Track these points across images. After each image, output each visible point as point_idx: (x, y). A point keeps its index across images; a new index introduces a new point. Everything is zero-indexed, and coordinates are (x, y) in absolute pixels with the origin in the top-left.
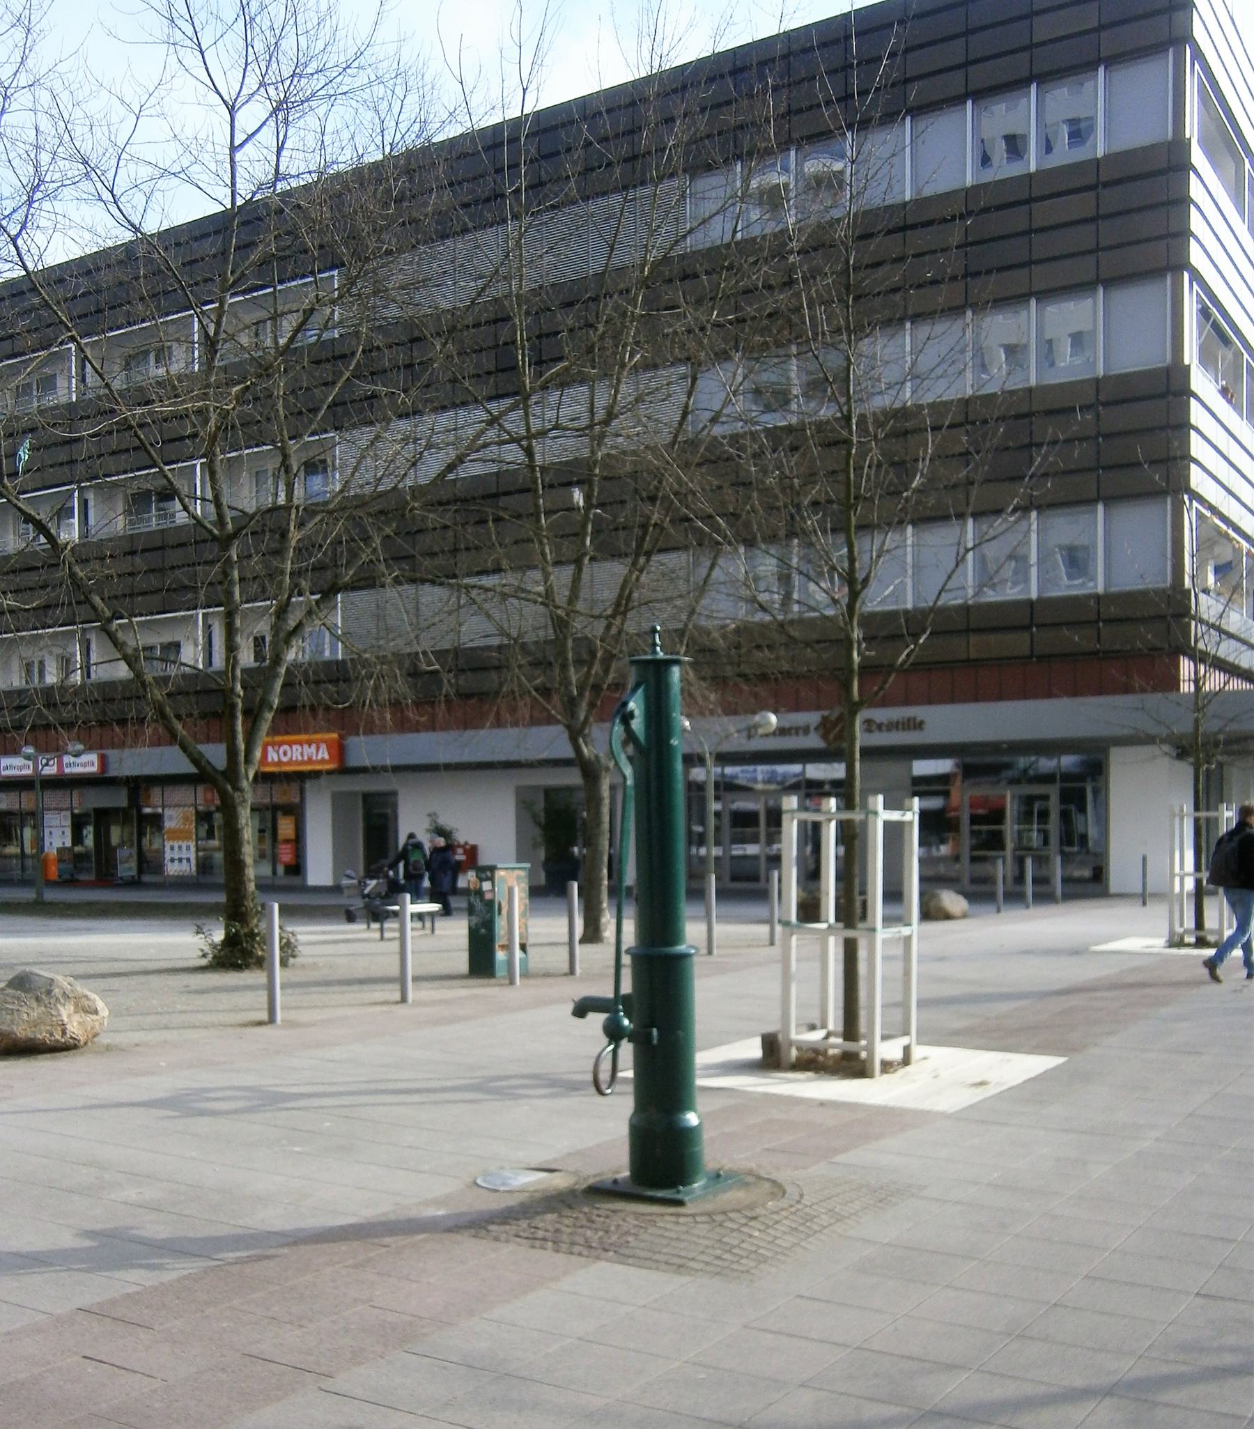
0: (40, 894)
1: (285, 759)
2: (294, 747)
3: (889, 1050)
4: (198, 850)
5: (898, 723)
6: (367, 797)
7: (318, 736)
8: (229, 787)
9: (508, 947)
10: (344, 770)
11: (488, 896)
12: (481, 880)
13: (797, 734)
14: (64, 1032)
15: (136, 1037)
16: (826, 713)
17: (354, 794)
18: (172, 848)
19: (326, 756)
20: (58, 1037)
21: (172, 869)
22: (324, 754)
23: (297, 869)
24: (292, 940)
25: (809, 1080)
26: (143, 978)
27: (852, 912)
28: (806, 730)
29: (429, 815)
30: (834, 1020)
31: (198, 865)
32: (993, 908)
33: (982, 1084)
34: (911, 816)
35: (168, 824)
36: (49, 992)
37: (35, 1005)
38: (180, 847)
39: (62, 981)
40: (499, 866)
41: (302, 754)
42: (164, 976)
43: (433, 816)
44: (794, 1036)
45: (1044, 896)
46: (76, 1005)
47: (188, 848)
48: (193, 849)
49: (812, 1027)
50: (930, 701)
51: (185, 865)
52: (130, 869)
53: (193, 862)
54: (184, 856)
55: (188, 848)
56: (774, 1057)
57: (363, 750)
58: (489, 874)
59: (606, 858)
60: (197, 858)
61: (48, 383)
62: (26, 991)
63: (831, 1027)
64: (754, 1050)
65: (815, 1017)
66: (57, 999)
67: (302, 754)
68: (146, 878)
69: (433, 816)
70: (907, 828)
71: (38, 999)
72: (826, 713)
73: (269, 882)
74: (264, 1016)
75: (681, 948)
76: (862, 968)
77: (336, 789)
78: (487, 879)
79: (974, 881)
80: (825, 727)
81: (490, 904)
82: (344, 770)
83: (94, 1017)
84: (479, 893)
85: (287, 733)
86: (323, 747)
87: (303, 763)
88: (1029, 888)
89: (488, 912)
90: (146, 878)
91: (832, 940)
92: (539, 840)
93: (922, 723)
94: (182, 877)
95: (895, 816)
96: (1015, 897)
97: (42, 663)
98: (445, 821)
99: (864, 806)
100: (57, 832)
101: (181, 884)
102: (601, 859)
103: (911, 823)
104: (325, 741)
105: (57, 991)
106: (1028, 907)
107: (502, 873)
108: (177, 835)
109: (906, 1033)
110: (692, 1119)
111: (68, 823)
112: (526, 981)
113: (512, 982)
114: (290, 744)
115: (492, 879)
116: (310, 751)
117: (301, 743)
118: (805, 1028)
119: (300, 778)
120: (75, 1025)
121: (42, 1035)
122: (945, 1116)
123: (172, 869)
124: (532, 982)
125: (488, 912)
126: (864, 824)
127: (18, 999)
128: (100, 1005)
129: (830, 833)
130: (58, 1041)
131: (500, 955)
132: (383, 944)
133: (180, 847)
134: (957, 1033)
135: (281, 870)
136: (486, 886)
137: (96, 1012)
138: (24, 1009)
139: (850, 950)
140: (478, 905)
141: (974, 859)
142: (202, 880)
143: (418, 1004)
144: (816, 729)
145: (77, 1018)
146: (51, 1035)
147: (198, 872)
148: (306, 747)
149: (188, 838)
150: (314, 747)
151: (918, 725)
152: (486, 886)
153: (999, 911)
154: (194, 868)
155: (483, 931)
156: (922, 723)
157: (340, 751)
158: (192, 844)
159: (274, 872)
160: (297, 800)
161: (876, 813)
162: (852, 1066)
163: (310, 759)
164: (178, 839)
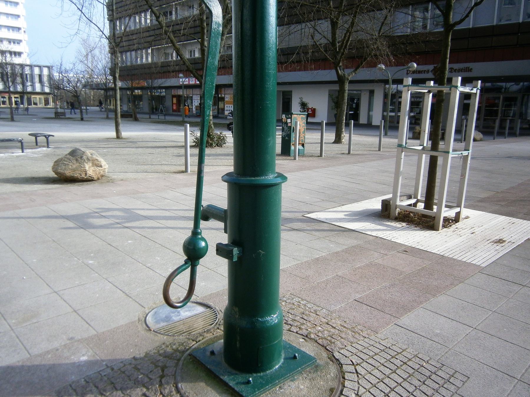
0: (183, 119)
3: (448, 213)
5: (462, 69)
9: (295, 145)
12: (287, 118)
13: (424, 73)
14: (86, 174)
15: (122, 176)
16: (436, 65)
20: (83, 176)
25: (402, 229)
26: (164, 150)
27: (438, 135)
28: (428, 72)
30: (421, 194)
32: (492, 138)
33: (500, 241)
34: (475, 90)
35: (226, 100)
36: (81, 157)
37: (75, 162)
39: (88, 152)
42: (177, 149)
43: (301, 98)
44: (398, 203)
45: (512, 134)
46: (93, 163)
49: (410, 197)
50: (475, 61)
56: (386, 213)
59: (345, 113)
62: (73, 156)
63: (419, 198)
64: (378, 206)
65: (411, 191)
66: (84, 160)
68: (220, 116)
69: (301, 98)
70: (472, 97)
71: (77, 160)
72: (436, 65)
74: (183, 168)
75: (270, 178)
76: (437, 189)
79: (484, 127)
80: (435, 71)
84: (286, 123)
88: (507, 132)
90: (220, 116)
91: (424, 155)
92: (334, 107)
93: (471, 69)
95: (467, 90)
96: (501, 134)
97: (194, 51)
98: (305, 100)
99: (450, 80)
100: (196, 101)
102: (343, 113)
103: (476, 94)
105: (84, 157)
106: (505, 138)
107: (295, 116)
108: (228, 103)
109: (459, 206)
110: (273, 319)
111: (199, 98)
113: (295, 159)
118: (405, 197)
120: (90, 170)
121: (77, 175)
122: (480, 270)
126: (449, 94)
127: (70, 159)
128: (103, 163)
129: (429, 100)
130: (83, 178)
131: (292, 148)
134: (482, 200)
136: (289, 121)
137: (101, 166)
138: (71, 164)
139: (433, 162)
140: (286, 128)
141: (485, 120)
144: (431, 71)
145: (92, 168)
146: (81, 175)
149: (231, 104)
151: (470, 70)
152: (289, 121)
153: (494, 139)
156: (471, 69)
161: (456, 87)
162: (428, 223)
164: (229, 104)
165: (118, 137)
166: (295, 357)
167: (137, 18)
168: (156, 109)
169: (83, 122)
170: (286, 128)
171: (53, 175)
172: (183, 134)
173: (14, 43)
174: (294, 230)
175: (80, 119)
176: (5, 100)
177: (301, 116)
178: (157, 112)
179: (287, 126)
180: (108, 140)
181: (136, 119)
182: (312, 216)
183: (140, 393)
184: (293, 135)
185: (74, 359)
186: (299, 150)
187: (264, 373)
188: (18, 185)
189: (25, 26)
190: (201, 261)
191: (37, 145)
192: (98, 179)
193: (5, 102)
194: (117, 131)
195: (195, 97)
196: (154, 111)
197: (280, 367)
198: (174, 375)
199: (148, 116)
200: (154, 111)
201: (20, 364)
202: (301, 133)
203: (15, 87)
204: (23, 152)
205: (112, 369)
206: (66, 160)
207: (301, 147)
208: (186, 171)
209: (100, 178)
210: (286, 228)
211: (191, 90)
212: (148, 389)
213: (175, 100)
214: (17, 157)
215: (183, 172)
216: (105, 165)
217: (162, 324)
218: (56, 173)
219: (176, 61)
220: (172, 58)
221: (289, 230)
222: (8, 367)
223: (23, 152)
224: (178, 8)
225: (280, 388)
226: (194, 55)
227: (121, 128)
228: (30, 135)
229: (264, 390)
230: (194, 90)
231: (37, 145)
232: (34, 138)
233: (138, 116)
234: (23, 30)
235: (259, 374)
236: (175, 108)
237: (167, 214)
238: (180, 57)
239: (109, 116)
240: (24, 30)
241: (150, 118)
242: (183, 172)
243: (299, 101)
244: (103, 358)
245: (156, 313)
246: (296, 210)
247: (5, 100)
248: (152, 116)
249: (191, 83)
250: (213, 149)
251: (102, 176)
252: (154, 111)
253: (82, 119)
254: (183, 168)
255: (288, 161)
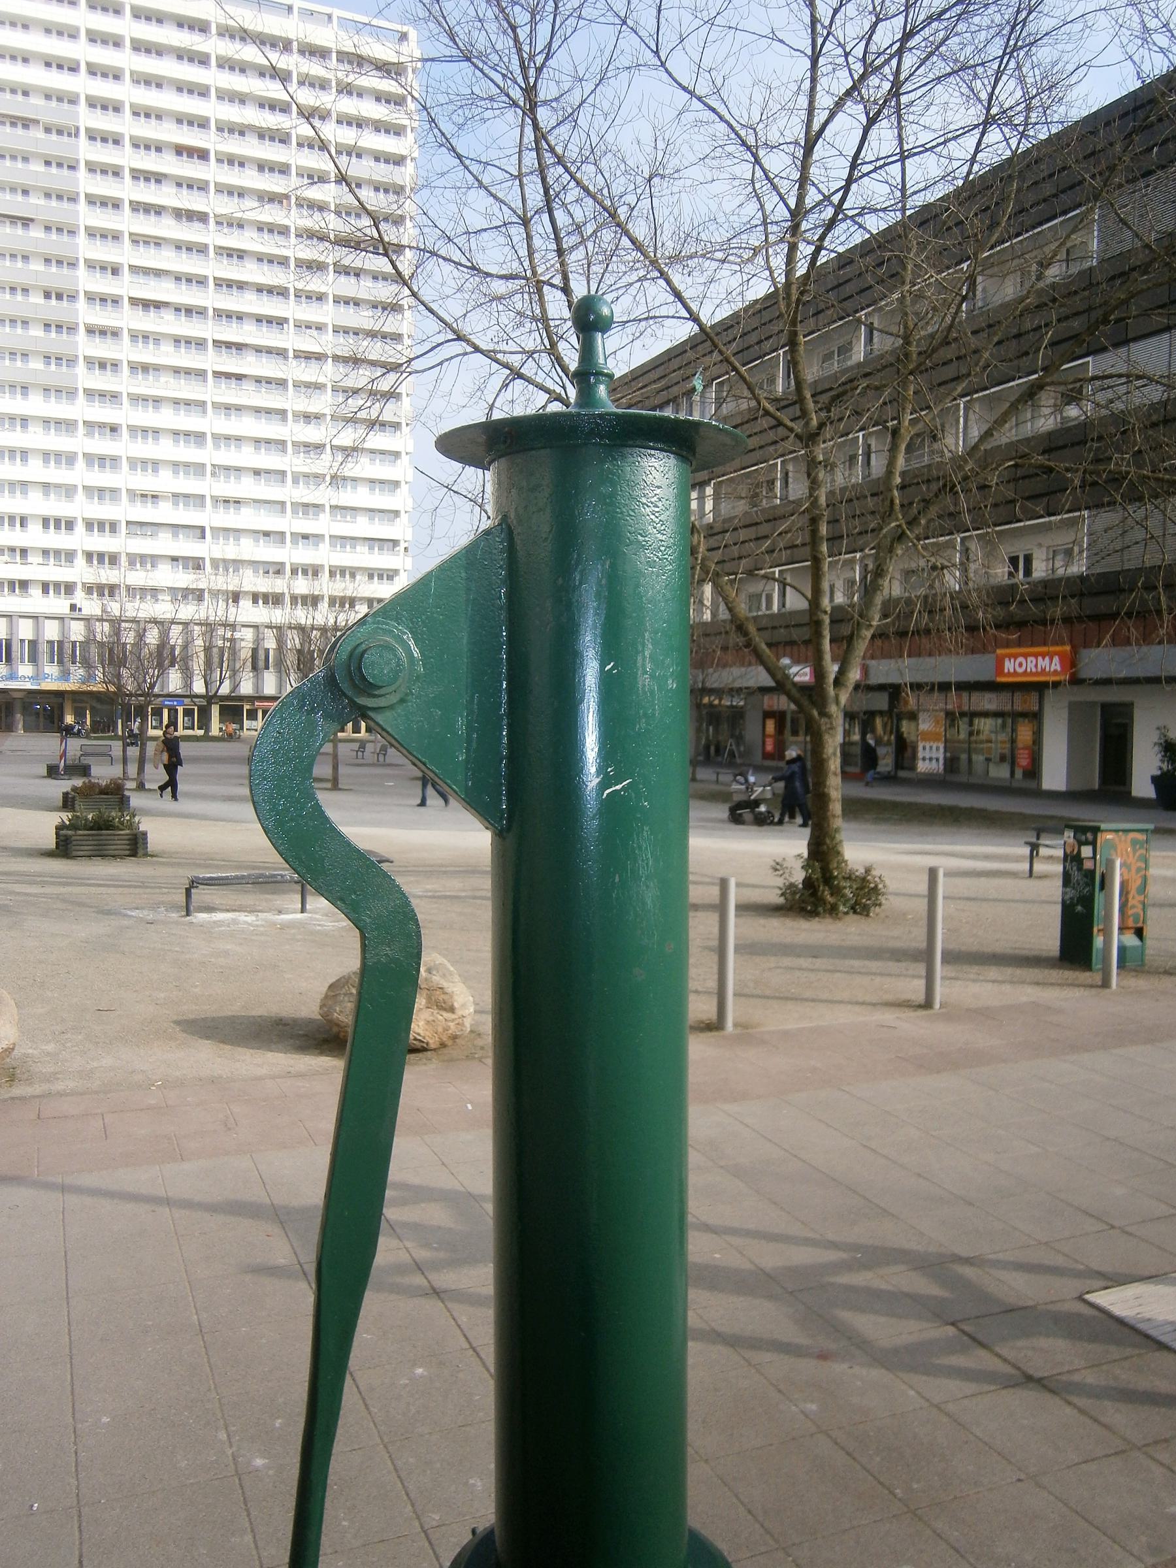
1: (1020, 670)
2: (1029, 659)
4: (945, 751)
6: (1106, 708)
7: (1052, 649)
8: (815, 713)
10: (1076, 681)
11: (1088, 865)
12: (1081, 843)
17: (1092, 704)
18: (924, 748)
19: (1059, 669)
21: (922, 767)
22: (1056, 665)
23: (1034, 772)
24: (880, 886)
29: (1158, 728)
31: (945, 764)
38: (931, 748)
40: (1103, 826)
41: (1036, 666)
43: (1163, 730)
47: (938, 749)
48: (942, 750)
51: (934, 764)
52: (887, 765)
53: (941, 761)
54: (934, 756)
55: (938, 749)
57: (1101, 660)
58: (1090, 836)
60: (945, 759)
61: (845, 350)
67: (1036, 666)
68: (902, 774)
69: (1163, 730)
73: (1008, 784)
77: (1073, 699)
78: (1087, 843)
81: (1091, 874)
82: (1076, 681)
83: (447, 1015)
85: (1032, 645)
86: (1056, 659)
87: (1036, 674)
89: (1087, 884)
94: (931, 774)
101: (929, 782)
104: (1056, 653)
107: (1109, 836)
112: (1133, 982)
113: (1106, 984)
114: (1026, 656)
115: (1094, 844)
116: (1044, 663)
117: (1036, 656)
119: (1040, 688)
123: (922, 767)
124: (1141, 983)
125: (1087, 884)
131: (1098, 941)
132: (1032, 883)
133: (931, 748)
135: (1019, 774)
136: (1086, 851)
137: (452, 1009)
140: (1076, 876)
142: (949, 778)
143: (953, 1013)
147: (945, 769)
148: (1040, 659)
149: (938, 740)
150: (1047, 659)
152: (1086, 851)
154: (941, 767)
155: (1079, 908)
157: (1071, 662)
158: (942, 746)
159: (1012, 773)
160: (1036, 708)
163: (1043, 670)
164: (929, 740)
170: (1076, 876)
173: (381, 577)
174: (1029, 1380)
177: (1132, 835)
178: (719, 759)
179: (1080, 869)
182: (1119, 1301)
184: (1099, 898)
186: (1122, 950)
189: (409, 537)
192: (443, 1045)
202: (1133, 892)
207: (1131, 940)
209: (450, 1043)
213: (770, 726)
214: (284, 926)
216: (464, 1006)
220: (769, 605)
221: (1009, 1383)
234: (403, 545)
236: (769, 747)
240: (406, 545)
243: (1155, 737)
246: (1060, 1261)
250: (839, 924)
251: (454, 1038)
255: (1078, 993)
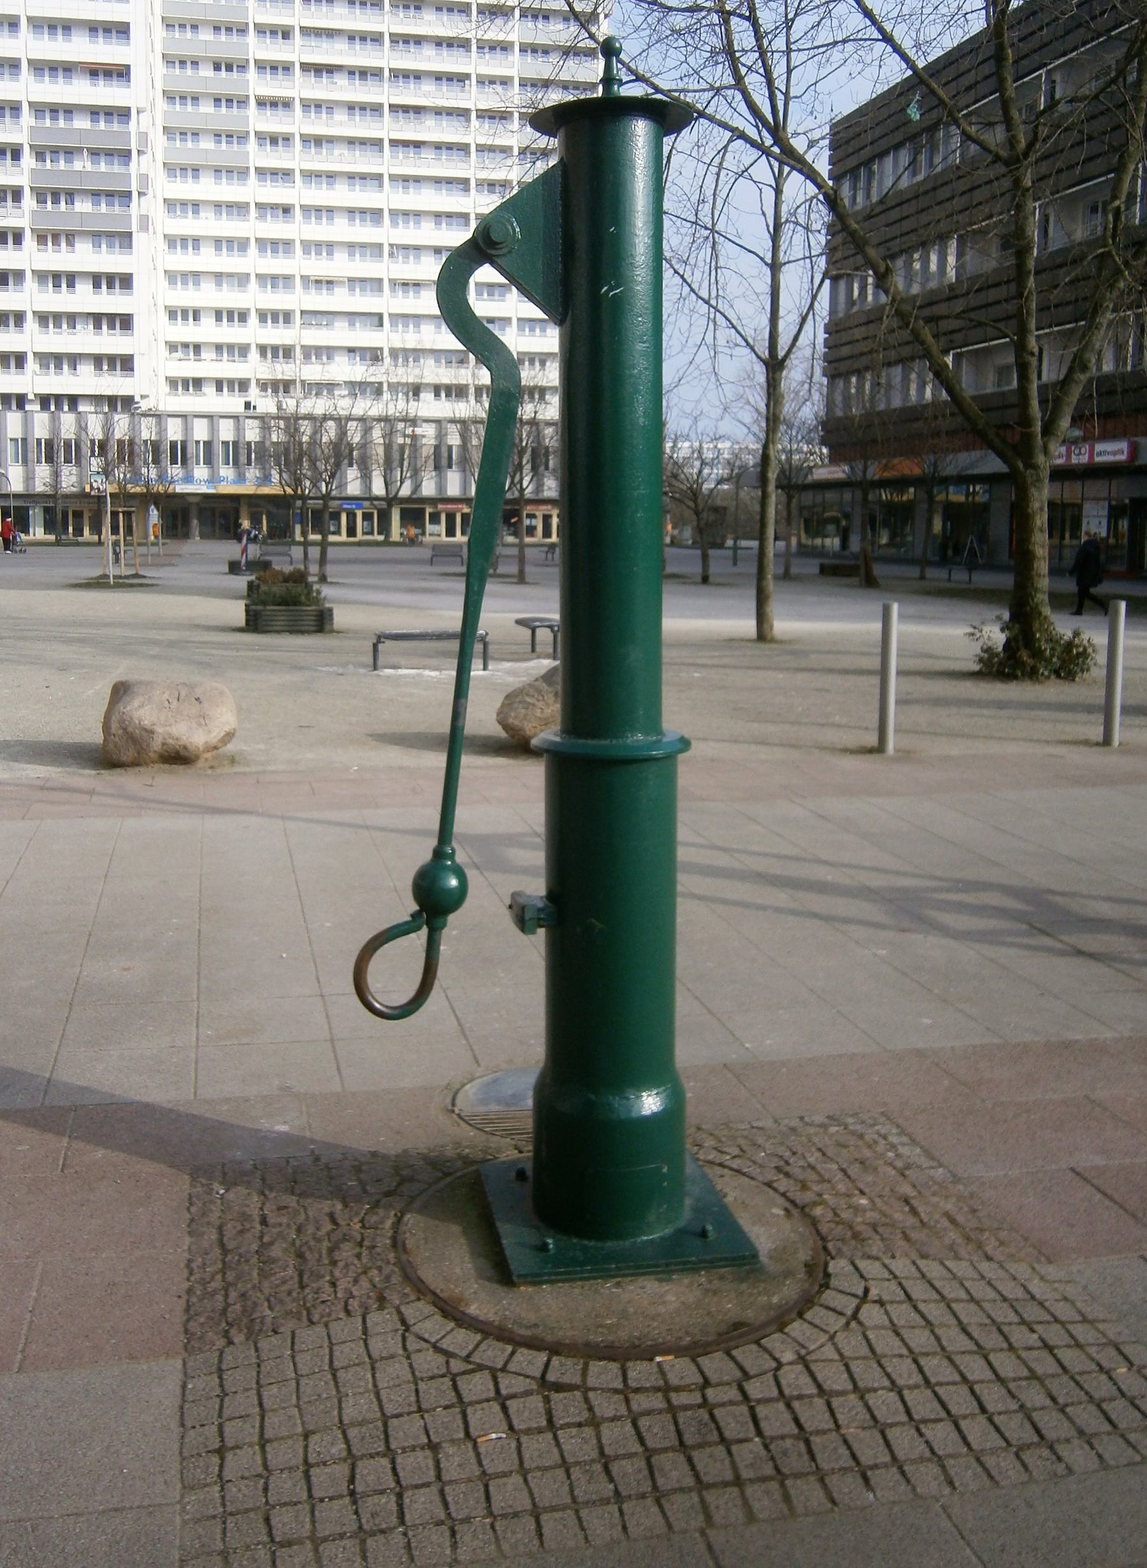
74: (872, 740)
138: (540, 704)
165: (763, 635)
166: (703, 1234)
167: (934, 258)
168: (957, 550)
169: (705, 589)
171: (498, 732)
172: (877, 626)
175: (699, 579)
176: (534, 522)
180: (732, 642)
181: (870, 582)
183: (327, 1210)
185: (265, 1124)
187: (599, 1244)
188: (414, 751)
190: (452, 918)
191: (533, 650)
193: (534, 528)
194: (762, 618)
195: (1088, 508)
196: (950, 552)
197: (652, 1241)
198: (413, 1199)
199: (915, 571)
200: (948, 552)
201: (170, 1106)
203: (539, 488)
204: (485, 669)
205: (317, 1159)
206: (532, 692)
208: (879, 749)
210: (1059, 945)
211: (1079, 483)
212: (346, 1206)
215: (871, 751)
217: (494, 1107)
218: (506, 727)
219: (935, 403)
221: (1062, 953)
222: (147, 1105)
223: (485, 669)
224: (1052, 219)
225: (618, 1284)
226: (1099, 368)
227: (775, 608)
228: (519, 622)
229: (569, 1273)
230: (1088, 483)
231: (533, 650)
232: (528, 632)
233: (878, 570)
235: (586, 1242)
237: (722, 860)
238: (950, 391)
239: (794, 570)
241: (922, 577)
242: (871, 751)
244: (317, 1137)
245: (495, 1081)
247: (534, 522)
248: (932, 573)
249: (1074, 460)
252: (950, 552)
253: (705, 580)
254: (872, 740)
